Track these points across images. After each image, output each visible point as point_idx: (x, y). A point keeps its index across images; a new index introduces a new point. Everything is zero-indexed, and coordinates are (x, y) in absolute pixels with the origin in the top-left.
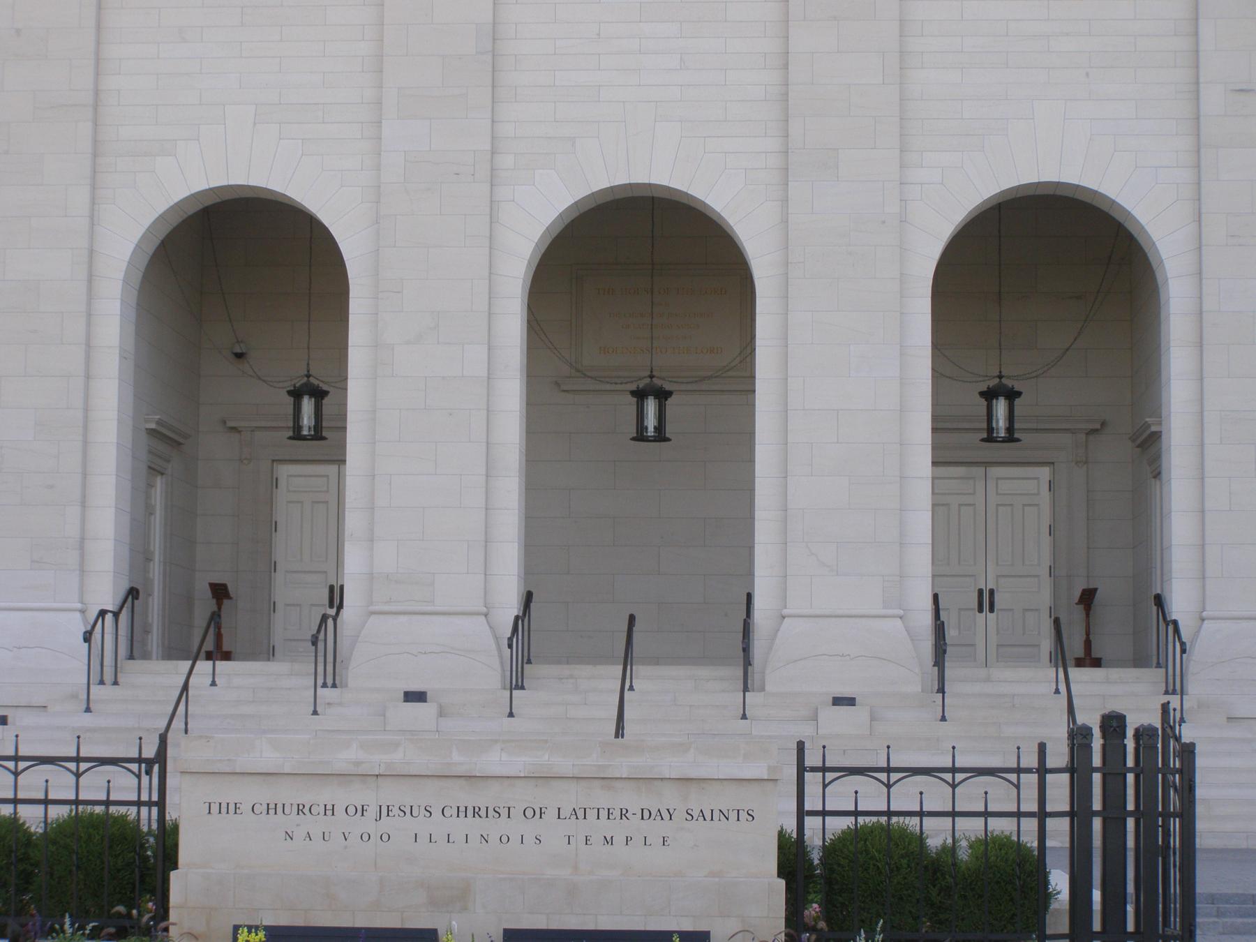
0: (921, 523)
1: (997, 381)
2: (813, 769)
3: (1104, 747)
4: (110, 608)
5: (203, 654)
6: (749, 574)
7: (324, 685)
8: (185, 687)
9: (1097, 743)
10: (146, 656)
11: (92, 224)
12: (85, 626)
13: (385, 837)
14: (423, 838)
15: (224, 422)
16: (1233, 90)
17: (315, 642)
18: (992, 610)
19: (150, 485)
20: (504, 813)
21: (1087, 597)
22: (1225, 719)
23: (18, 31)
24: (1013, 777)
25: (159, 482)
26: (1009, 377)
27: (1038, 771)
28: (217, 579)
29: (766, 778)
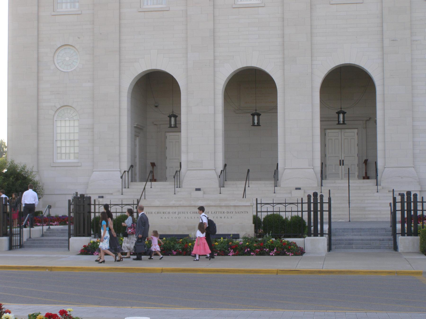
1: (340, 109)
2: (259, 204)
3: (407, 198)
4: (126, 170)
5: (149, 180)
7: (177, 187)
8: (144, 189)
9: (406, 197)
10: (135, 181)
11: (120, 79)
12: (121, 175)
13: (179, 218)
15: (153, 123)
16: (391, 40)
17: (174, 177)
18: (343, 165)
19: (135, 140)
21: (366, 162)
22: (388, 191)
23: (101, 33)
24: (297, 204)
25: (137, 138)
26: (343, 109)
27: (301, 203)
28: (152, 162)
29: (250, 205)
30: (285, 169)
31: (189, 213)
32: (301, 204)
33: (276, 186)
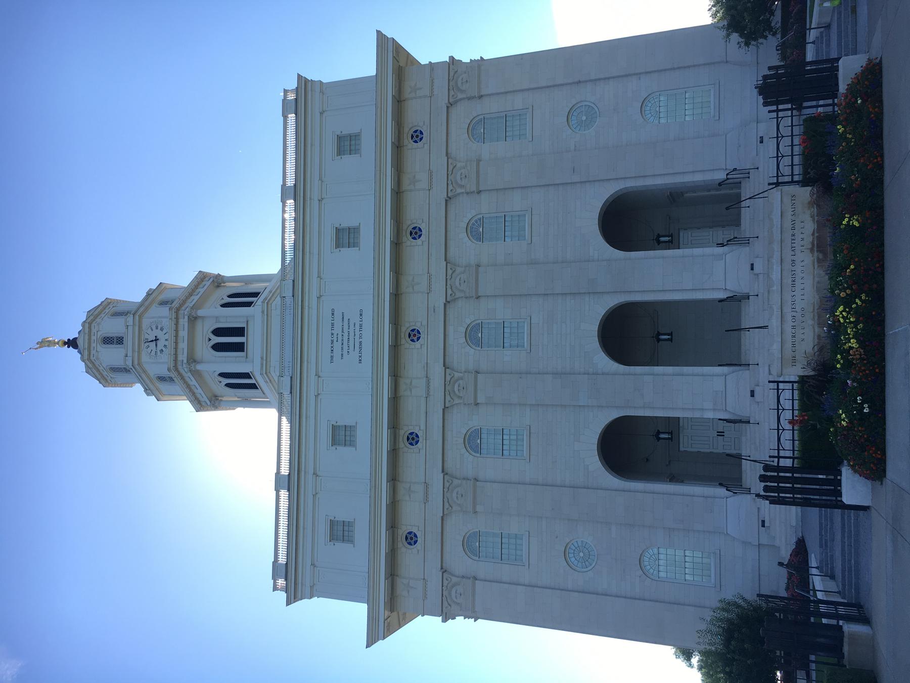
0: (697, 251)
6: (713, 300)
7: (750, 491)
14: (803, 297)
18: (718, 435)
20: (794, 272)
24: (780, 391)
30: (727, 533)
31: (794, 293)
32: (781, 460)
33: (749, 422)
